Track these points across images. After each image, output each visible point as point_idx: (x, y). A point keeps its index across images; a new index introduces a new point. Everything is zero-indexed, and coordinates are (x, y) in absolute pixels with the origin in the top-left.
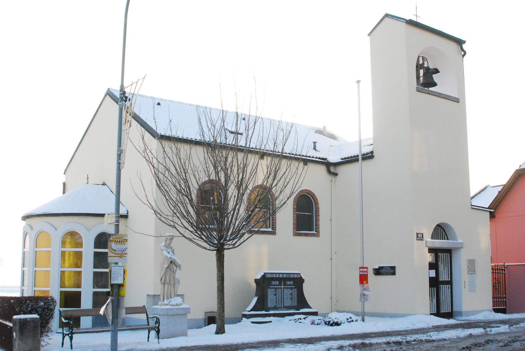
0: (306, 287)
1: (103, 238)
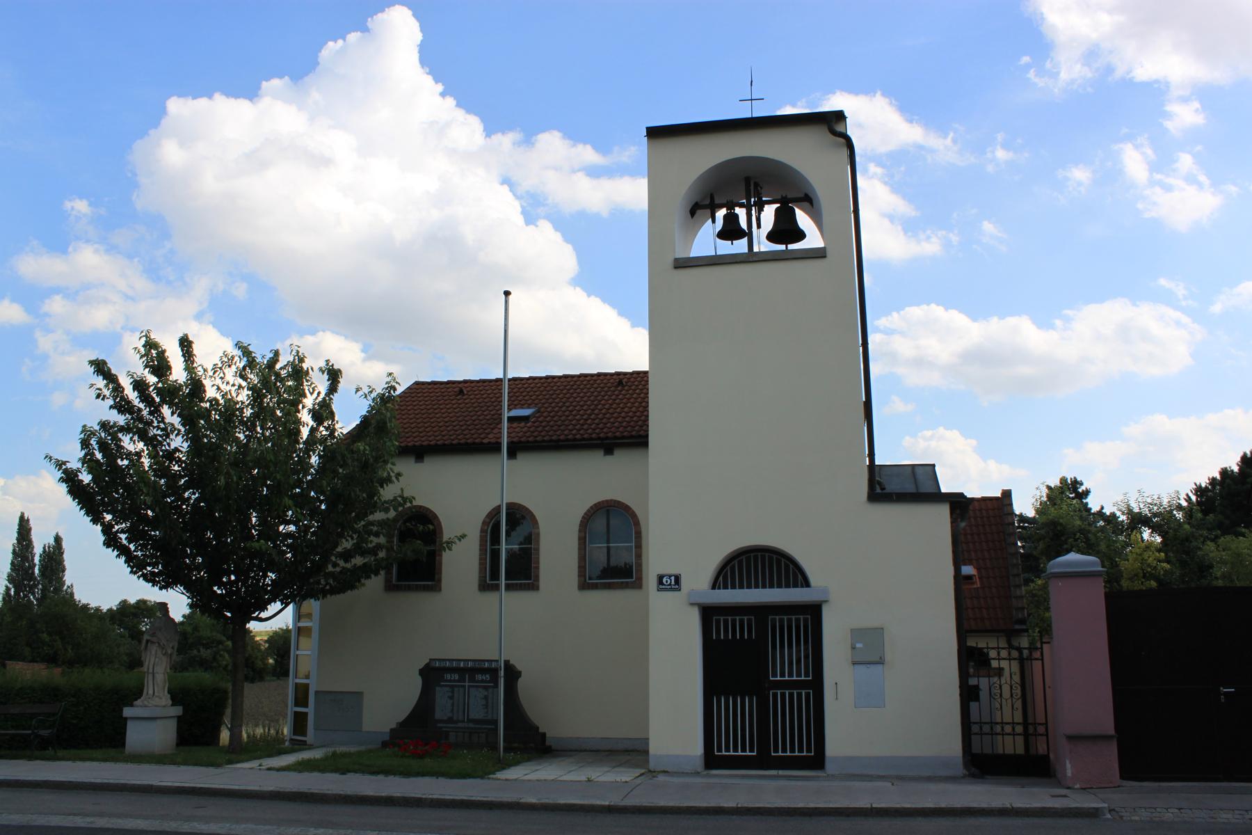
0: (521, 683)
1: (335, 565)
